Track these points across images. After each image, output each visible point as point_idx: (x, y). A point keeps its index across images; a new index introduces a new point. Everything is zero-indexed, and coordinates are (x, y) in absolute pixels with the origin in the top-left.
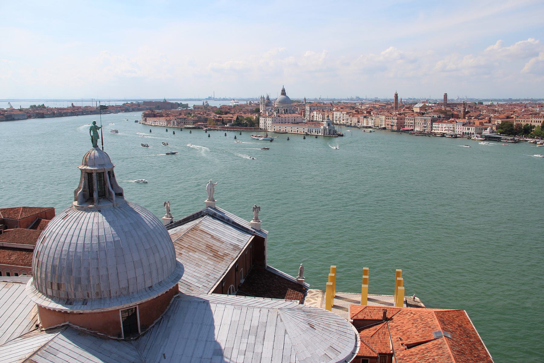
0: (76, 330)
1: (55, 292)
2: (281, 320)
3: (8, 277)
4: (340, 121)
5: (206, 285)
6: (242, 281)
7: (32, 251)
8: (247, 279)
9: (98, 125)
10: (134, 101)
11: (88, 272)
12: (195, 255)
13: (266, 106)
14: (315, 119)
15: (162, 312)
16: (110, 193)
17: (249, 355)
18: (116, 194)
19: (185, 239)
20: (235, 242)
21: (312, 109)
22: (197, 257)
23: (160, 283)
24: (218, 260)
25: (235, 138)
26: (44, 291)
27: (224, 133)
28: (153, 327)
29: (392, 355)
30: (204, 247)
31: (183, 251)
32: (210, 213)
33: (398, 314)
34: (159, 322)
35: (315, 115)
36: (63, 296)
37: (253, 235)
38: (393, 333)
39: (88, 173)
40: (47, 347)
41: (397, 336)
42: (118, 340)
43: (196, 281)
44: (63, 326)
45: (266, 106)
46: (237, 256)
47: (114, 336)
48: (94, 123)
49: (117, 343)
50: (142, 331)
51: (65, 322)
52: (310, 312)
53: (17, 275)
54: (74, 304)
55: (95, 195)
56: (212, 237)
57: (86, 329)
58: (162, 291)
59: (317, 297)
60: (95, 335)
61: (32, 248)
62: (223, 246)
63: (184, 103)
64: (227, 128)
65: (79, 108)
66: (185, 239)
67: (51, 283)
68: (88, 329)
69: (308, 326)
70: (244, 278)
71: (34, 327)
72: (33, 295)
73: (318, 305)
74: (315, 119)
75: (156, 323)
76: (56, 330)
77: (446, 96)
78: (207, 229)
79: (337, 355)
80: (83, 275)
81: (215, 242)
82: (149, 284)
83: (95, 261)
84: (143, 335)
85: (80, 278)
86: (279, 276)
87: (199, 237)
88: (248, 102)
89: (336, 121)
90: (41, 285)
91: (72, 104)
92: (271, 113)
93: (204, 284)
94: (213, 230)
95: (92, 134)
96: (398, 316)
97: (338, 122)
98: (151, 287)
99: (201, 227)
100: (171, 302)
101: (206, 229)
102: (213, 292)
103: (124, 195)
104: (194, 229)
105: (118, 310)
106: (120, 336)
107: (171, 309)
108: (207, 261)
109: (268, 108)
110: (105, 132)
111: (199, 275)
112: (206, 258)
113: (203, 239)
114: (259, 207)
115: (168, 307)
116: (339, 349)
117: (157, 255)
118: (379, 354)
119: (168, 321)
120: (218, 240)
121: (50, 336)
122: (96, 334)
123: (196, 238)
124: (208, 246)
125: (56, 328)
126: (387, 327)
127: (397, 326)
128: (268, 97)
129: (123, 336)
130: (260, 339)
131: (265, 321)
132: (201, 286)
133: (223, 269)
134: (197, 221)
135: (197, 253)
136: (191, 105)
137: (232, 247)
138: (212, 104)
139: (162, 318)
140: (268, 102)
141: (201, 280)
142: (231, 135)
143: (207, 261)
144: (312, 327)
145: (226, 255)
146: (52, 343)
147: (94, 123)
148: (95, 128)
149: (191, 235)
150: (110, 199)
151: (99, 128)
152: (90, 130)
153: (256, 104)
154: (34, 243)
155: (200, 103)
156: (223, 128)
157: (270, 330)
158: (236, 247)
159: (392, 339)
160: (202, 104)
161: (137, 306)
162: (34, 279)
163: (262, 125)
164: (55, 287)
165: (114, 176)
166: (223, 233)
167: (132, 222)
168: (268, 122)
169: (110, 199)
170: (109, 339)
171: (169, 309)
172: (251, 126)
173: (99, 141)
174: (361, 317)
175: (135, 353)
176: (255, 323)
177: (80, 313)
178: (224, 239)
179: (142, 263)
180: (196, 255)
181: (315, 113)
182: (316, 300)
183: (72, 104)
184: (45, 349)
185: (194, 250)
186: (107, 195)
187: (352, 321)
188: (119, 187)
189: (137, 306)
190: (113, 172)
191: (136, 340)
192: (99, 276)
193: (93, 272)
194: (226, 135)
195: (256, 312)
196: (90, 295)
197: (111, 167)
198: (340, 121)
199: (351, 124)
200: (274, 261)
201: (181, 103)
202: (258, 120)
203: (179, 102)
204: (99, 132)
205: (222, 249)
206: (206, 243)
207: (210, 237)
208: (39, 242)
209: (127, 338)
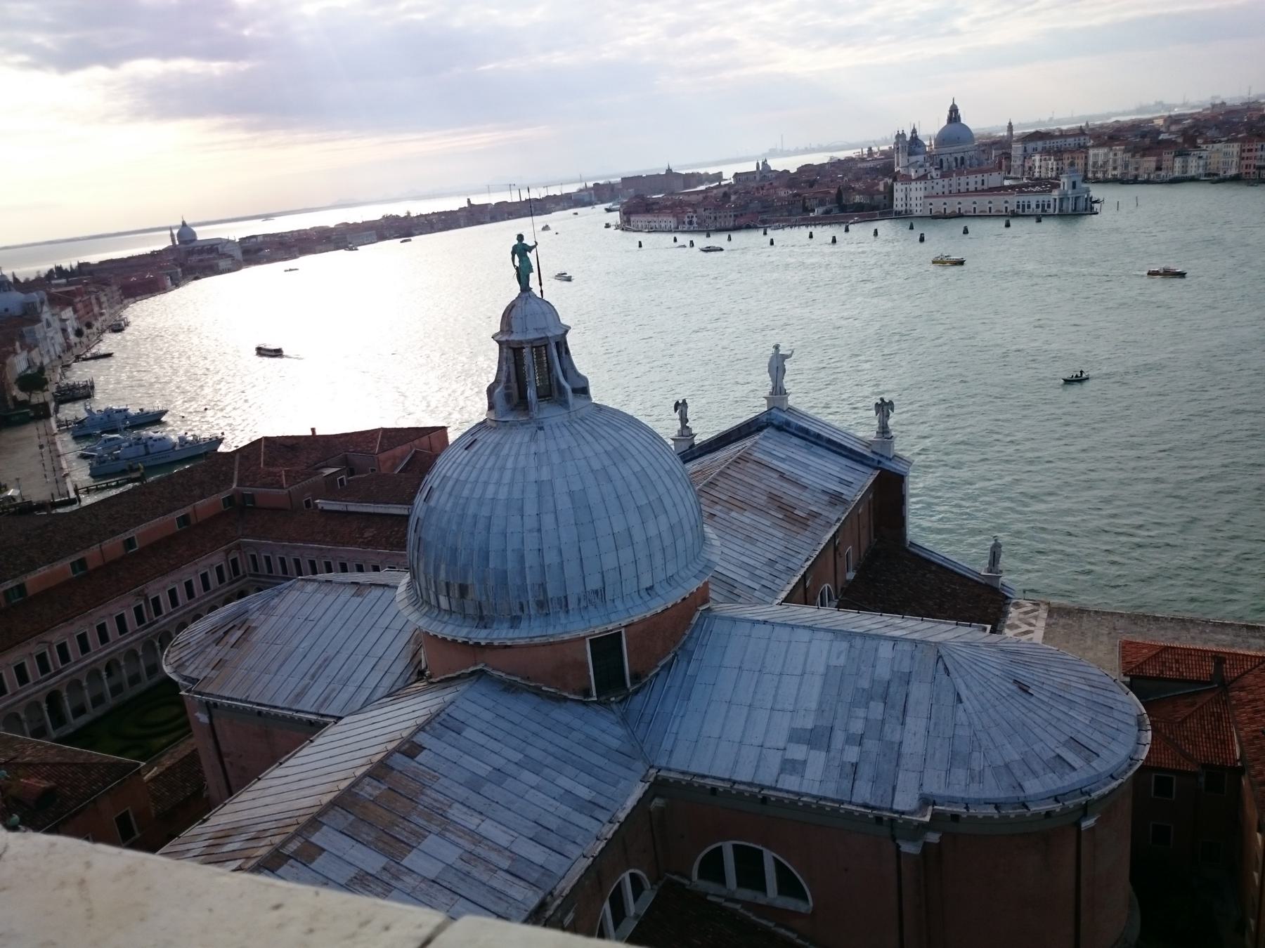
0: (500, 681)
1: (454, 602)
2: (946, 669)
3: (360, 574)
4: (1105, 173)
5: (769, 584)
6: (851, 576)
7: (407, 517)
8: (862, 570)
9: (528, 241)
10: (601, 178)
11: (522, 559)
12: (743, 519)
13: (910, 154)
14: (1037, 175)
15: (675, 643)
16: (561, 389)
17: (871, 745)
18: (575, 391)
19: (722, 483)
20: (834, 487)
21: (1030, 151)
22: (747, 521)
23: (669, 580)
24: (795, 529)
25: (834, 241)
26: (433, 602)
27: (805, 231)
28: (657, 674)
29: (1241, 771)
30: (762, 500)
31: (716, 510)
32: (775, 422)
33: (1256, 671)
34: (668, 666)
35: (1037, 164)
36: (471, 610)
37: (876, 468)
38: (1244, 717)
39: (514, 349)
40: (443, 715)
41: (1254, 727)
42: (585, 703)
43: (746, 574)
44: (473, 673)
45: (910, 154)
46: (839, 519)
47: (575, 693)
48: (520, 237)
49: (581, 709)
50: (633, 684)
51: (476, 664)
52: (1018, 653)
53: (376, 569)
54: (495, 626)
55: (531, 393)
56: (782, 476)
57: (518, 679)
58: (675, 596)
59: (1036, 618)
60: (537, 692)
61: (406, 512)
62: (806, 495)
63: (712, 171)
64: (815, 219)
65: (484, 207)
66: (722, 483)
67: (447, 585)
68: (522, 678)
69: (1014, 687)
70: (855, 568)
71: (414, 677)
72: (411, 609)
73: (1038, 636)
74: (1037, 175)
75: (663, 667)
76: (457, 682)
77: (1010, 127)
78: (766, 458)
79: (1088, 761)
80: (511, 565)
81: (793, 491)
82: (646, 582)
83: (536, 534)
84: (636, 692)
85: (505, 572)
86: (940, 566)
87: (752, 476)
88: (865, 151)
89: (1094, 173)
90: (427, 589)
91: (469, 201)
92: (921, 172)
93: (764, 582)
94: (783, 460)
95: (517, 264)
96: (1256, 677)
97: (1100, 175)
98: (652, 588)
99: (758, 455)
100: (694, 621)
101: (766, 458)
102: (786, 600)
103: (592, 391)
104: (742, 459)
105: (584, 638)
106: (587, 693)
107: (695, 635)
108: (771, 531)
109: (913, 159)
110: (547, 259)
111: (752, 562)
112: (768, 523)
113: (760, 480)
114: (891, 403)
115: (687, 632)
116: (1093, 746)
117: (662, 519)
118: (1204, 766)
119: (689, 662)
120: (795, 483)
121: (448, 695)
122: (540, 689)
123: (747, 479)
124: (773, 497)
125: (458, 677)
126: (1225, 703)
127: (1256, 700)
128: (914, 131)
129: (594, 693)
130: (897, 712)
131: (880, 718)
132: (757, 587)
133: (805, 550)
134: (748, 443)
135: (746, 513)
136: (728, 175)
137: (827, 498)
138: (777, 165)
139: (676, 654)
140: (911, 144)
141: (757, 572)
142: (824, 233)
143: (771, 531)
144: (1024, 689)
145: (815, 515)
146: (452, 707)
147: (520, 237)
148: (521, 250)
149: (734, 474)
150: (564, 403)
151: (530, 249)
152: (513, 253)
153: (883, 153)
154: (409, 501)
155: (751, 167)
156: (804, 219)
157: (919, 692)
158: (836, 499)
159: (1243, 734)
160: (754, 169)
161: (623, 630)
162: (414, 577)
163: (898, 205)
164: (455, 593)
165: (567, 351)
166: (806, 466)
167: (609, 448)
168: (913, 194)
169: (564, 403)
170: (566, 699)
171: (690, 637)
172: (876, 207)
173: (533, 277)
174: (1151, 671)
175: (619, 731)
176: (883, 672)
177: (507, 647)
178: (807, 479)
179: (631, 536)
180: (747, 518)
181: (1037, 158)
182: (1030, 625)
183: (469, 201)
184: (438, 719)
185: (743, 505)
186: (556, 394)
187: (1128, 679)
188: (579, 375)
189: (623, 630)
190: (566, 343)
191: (620, 702)
192: (542, 566)
193: (531, 560)
194: (811, 236)
195: (885, 650)
196: (526, 609)
197: (561, 332)
198: (1105, 173)
199: (1136, 177)
200: (929, 525)
201: (707, 174)
202: (890, 191)
203: (702, 171)
204: (531, 256)
205: (808, 502)
206: (769, 489)
207: (775, 475)
208: (419, 499)
209: (603, 698)
